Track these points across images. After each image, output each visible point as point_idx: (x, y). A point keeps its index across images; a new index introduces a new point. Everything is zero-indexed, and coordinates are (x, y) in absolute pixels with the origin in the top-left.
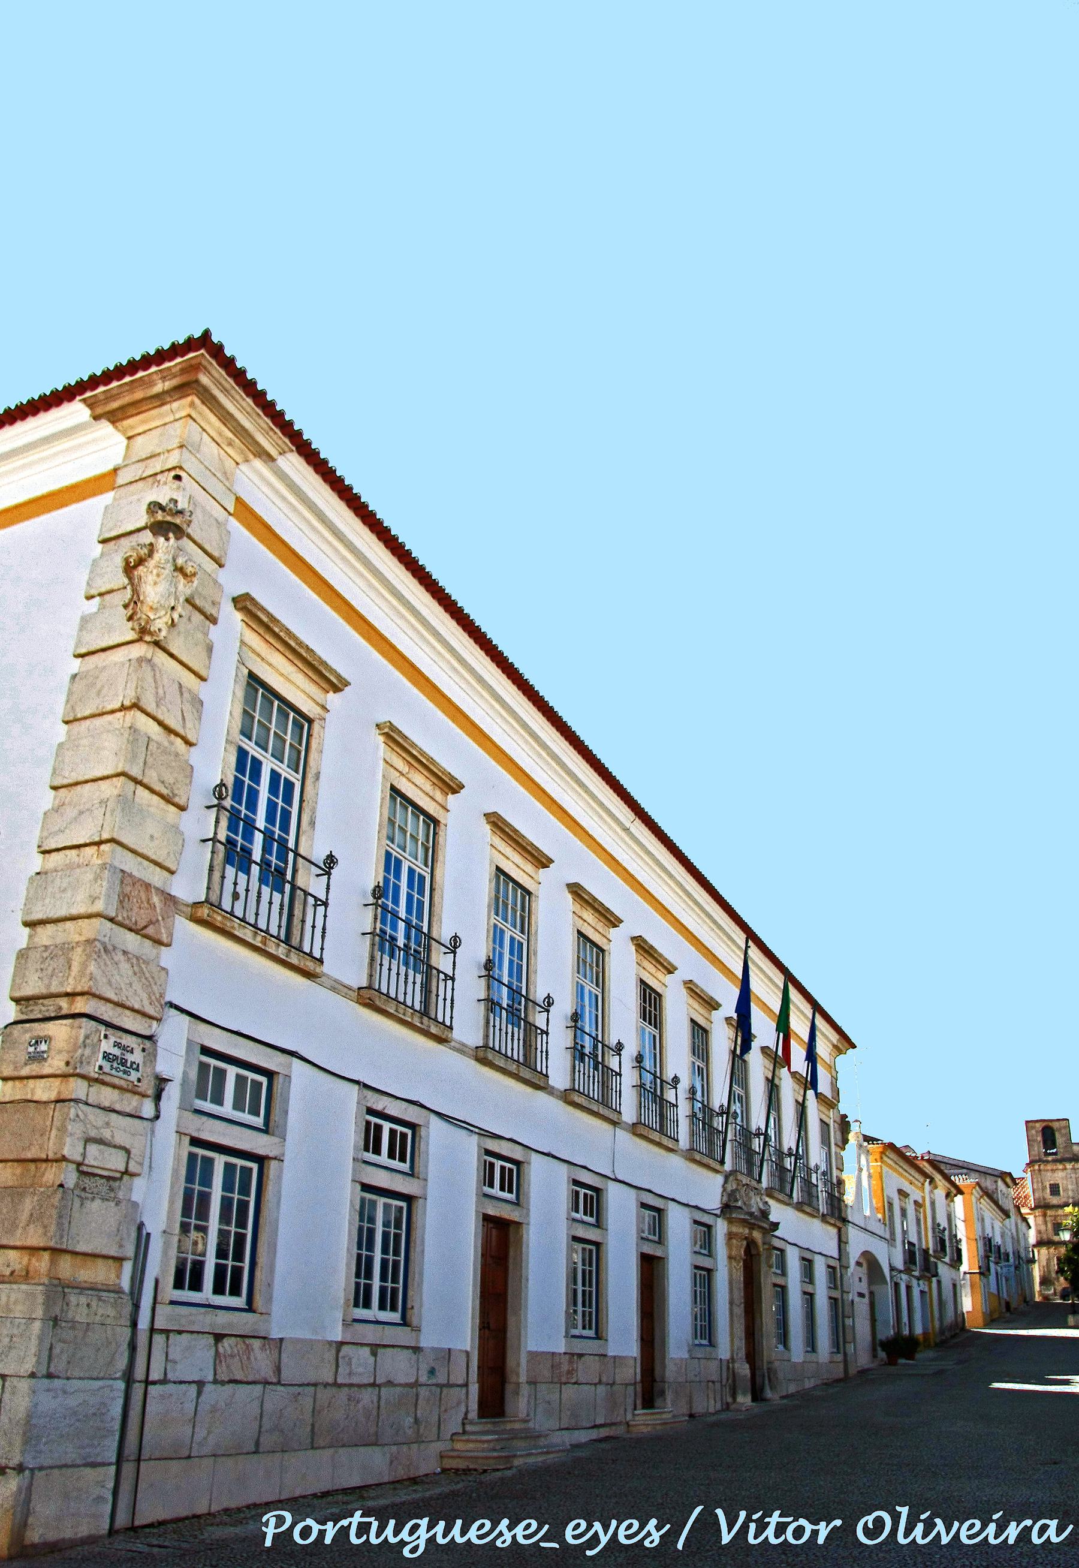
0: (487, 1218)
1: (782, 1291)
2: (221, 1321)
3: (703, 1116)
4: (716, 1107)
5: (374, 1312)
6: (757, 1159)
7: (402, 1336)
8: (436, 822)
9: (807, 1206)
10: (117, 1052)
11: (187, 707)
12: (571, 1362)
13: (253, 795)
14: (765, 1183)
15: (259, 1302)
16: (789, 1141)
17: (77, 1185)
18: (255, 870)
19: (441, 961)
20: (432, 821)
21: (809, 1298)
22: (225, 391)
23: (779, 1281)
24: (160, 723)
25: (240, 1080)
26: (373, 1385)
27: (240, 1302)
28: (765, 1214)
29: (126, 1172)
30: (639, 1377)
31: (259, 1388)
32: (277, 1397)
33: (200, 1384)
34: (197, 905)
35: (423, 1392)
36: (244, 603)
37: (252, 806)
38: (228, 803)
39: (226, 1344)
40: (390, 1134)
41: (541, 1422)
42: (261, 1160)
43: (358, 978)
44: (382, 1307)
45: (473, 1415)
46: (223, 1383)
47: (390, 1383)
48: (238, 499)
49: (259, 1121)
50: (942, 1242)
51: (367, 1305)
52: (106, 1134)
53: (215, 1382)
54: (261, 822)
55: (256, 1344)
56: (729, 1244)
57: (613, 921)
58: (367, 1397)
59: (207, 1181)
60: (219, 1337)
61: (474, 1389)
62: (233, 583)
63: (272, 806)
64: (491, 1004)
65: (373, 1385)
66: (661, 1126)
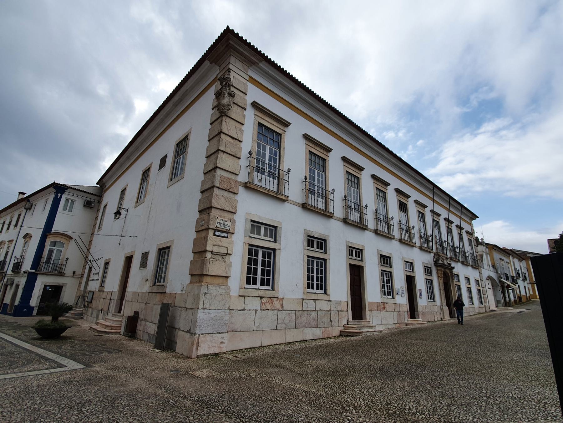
0: (351, 265)
1: (459, 287)
2: (261, 293)
3: (425, 238)
4: (429, 235)
5: (315, 290)
6: (457, 254)
7: (325, 297)
8: (325, 160)
9: (465, 263)
10: (221, 222)
11: (238, 132)
12: (384, 305)
13: (314, 178)
14: (449, 256)
15: (276, 289)
16: (457, 243)
17: (211, 258)
18: (316, 194)
19: (391, 223)
20: (358, 178)
21: (469, 289)
22: (238, 45)
23: (458, 283)
24: (230, 136)
25: (356, 251)
26: (315, 310)
27: (270, 288)
28: (450, 264)
29: (227, 254)
30: (409, 310)
31: (276, 311)
32: (282, 315)
33: (256, 311)
34: (246, 183)
35: (332, 313)
36: (255, 105)
37: (314, 180)
38: (308, 180)
39: (264, 300)
40: (316, 243)
41: (373, 323)
42: (274, 250)
43: (301, 200)
44: (318, 289)
45: (350, 319)
46: (264, 310)
47: (321, 310)
48: (249, 76)
49: (323, 251)
50: (519, 274)
51: (313, 288)
52: (220, 244)
53: (261, 310)
54: (317, 184)
55: (275, 299)
56: (437, 273)
57: (408, 197)
58: (313, 314)
59: (313, 265)
60: (261, 298)
61: (350, 312)
62: (249, 99)
63: (318, 180)
64: (401, 229)
65: (315, 310)
66: (388, 231)
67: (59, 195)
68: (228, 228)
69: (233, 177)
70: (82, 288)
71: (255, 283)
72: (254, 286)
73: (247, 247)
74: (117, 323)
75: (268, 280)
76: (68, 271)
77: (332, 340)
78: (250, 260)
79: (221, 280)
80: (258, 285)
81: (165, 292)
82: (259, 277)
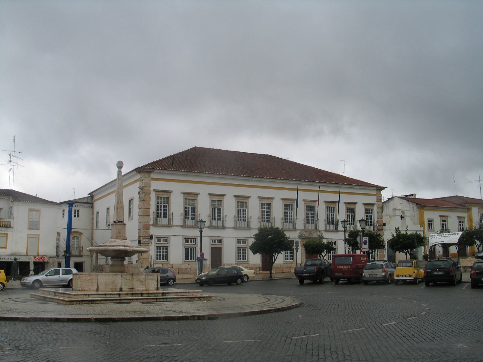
15: (168, 260)
42: (195, 247)
60: (163, 264)
67: (71, 208)
68: (147, 242)
69: (147, 223)
70: (94, 263)
71: (188, 259)
72: (240, 261)
73: (156, 248)
74: (92, 274)
75: (373, 258)
76: (85, 253)
77: (382, 281)
78: (186, 252)
79: (147, 259)
80: (189, 260)
81: (132, 264)
82: (289, 257)
